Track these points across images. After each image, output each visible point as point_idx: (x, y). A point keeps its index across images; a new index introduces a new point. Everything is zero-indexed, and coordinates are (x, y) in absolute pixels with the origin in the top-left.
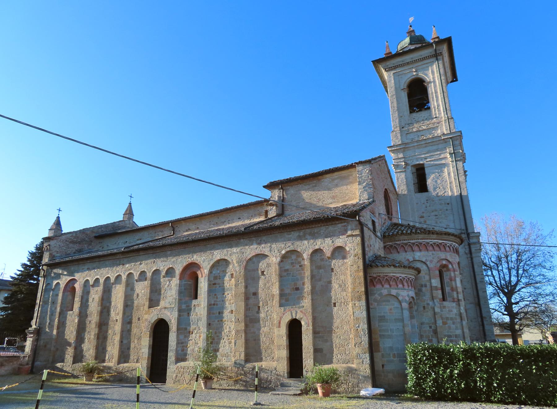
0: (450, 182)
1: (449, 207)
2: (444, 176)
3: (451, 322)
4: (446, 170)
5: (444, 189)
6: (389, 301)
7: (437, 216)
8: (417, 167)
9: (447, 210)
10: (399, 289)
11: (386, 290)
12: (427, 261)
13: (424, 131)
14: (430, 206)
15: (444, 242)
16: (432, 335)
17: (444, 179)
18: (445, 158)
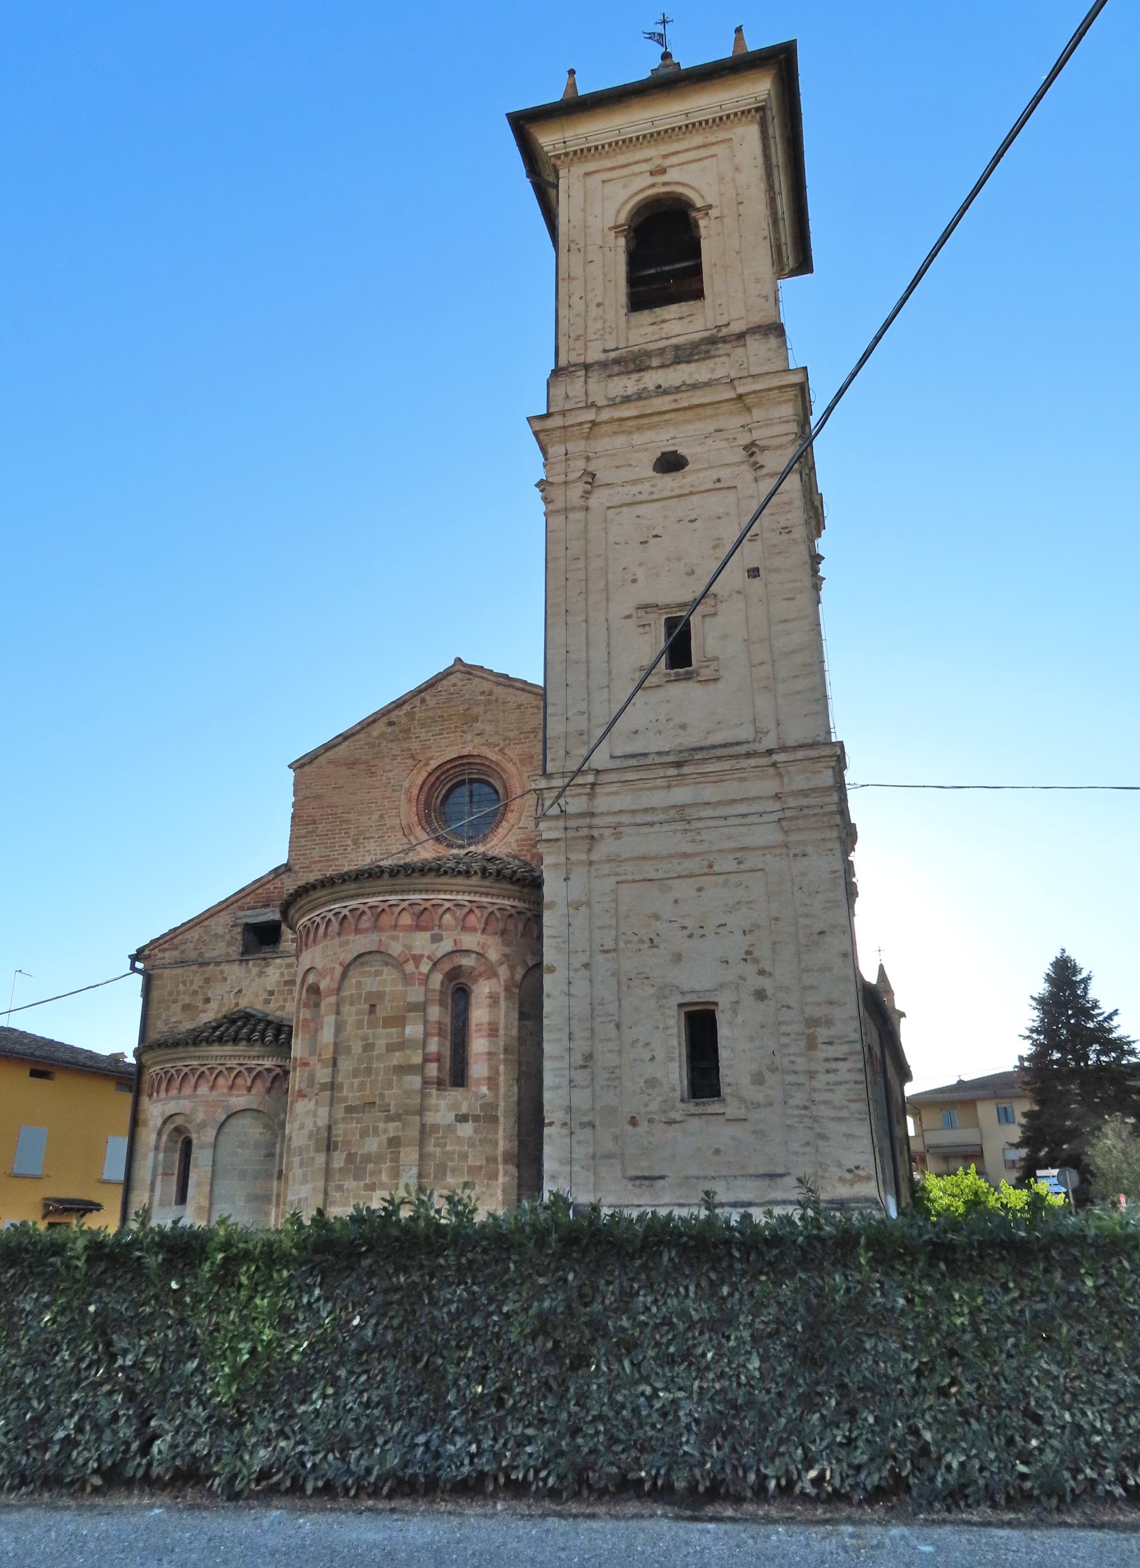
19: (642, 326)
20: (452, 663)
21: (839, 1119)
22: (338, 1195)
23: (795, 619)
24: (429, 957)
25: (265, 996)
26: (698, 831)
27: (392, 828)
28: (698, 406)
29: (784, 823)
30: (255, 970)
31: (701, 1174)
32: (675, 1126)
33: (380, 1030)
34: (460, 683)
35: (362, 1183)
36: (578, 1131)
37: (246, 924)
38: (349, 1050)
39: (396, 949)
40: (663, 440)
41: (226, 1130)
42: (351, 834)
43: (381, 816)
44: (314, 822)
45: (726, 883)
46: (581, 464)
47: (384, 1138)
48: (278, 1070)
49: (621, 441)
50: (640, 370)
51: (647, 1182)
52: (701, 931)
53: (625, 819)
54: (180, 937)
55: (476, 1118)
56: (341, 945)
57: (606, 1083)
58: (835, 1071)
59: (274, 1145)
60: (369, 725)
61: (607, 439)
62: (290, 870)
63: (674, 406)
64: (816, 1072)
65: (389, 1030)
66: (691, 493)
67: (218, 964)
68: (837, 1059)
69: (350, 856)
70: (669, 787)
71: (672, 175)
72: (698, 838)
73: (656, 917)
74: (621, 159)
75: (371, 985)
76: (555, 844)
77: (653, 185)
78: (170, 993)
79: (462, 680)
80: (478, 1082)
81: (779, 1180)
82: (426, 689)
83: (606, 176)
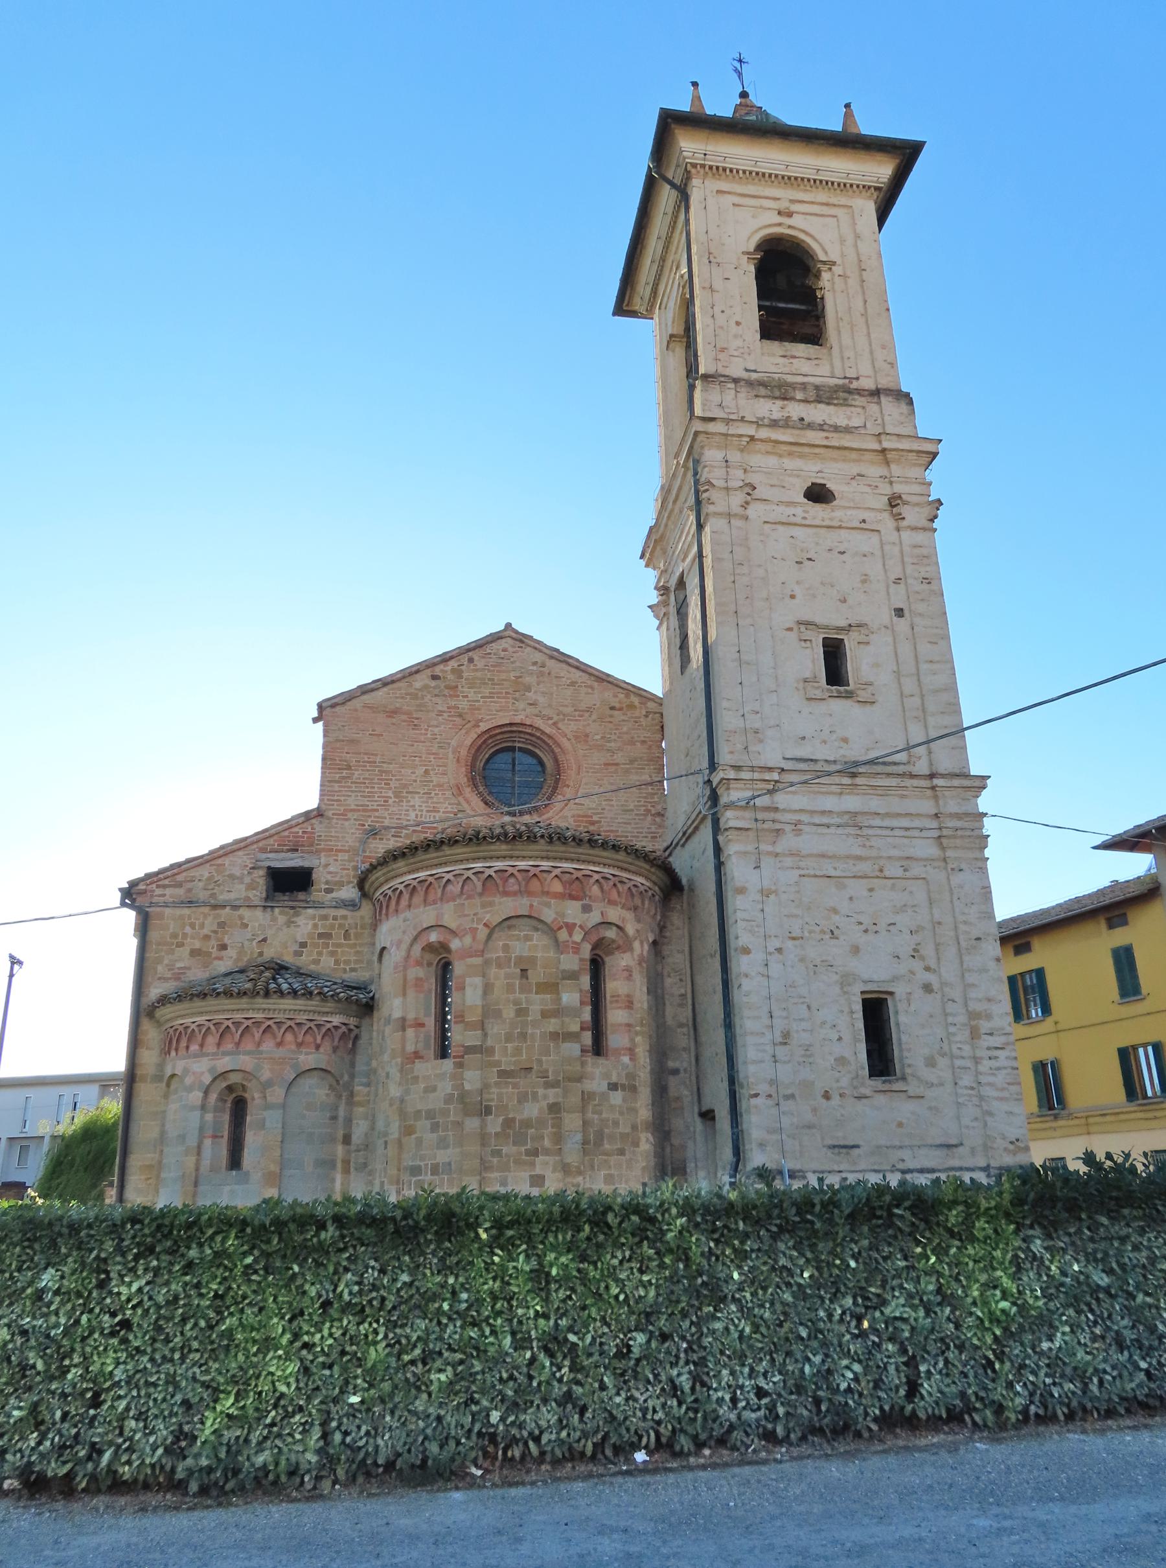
15: (434, 872)
19: (774, 355)
20: (502, 628)
21: (1001, 1099)
22: (495, 1160)
23: (938, 662)
24: (581, 927)
25: (296, 947)
26: (868, 837)
27: (440, 785)
28: (846, 448)
29: (944, 841)
30: (282, 919)
31: (888, 1144)
32: (864, 1101)
33: (533, 996)
34: (511, 649)
35: (523, 1149)
36: (782, 1102)
37: (269, 868)
38: (498, 1014)
39: (548, 915)
40: (814, 471)
41: (293, 1090)
42: (392, 785)
43: (426, 772)
44: (349, 767)
45: (893, 887)
46: (740, 473)
47: (544, 1104)
48: (344, 1028)
49: (772, 461)
50: (785, 399)
51: (844, 1151)
52: (875, 928)
53: (805, 818)
54: (184, 874)
55: (623, 1087)
56: (483, 906)
57: (802, 1059)
58: (996, 1058)
59: (337, 1108)
60: (411, 674)
61: (759, 456)
62: (322, 815)
63: (825, 443)
64: (981, 1058)
65: (542, 996)
66: (840, 527)
67: (235, 908)
68: (996, 1048)
69: (391, 809)
70: (841, 793)
71: (796, 221)
72: (868, 844)
73: (835, 911)
74: (751, 189)
75: (519, 949)
76: (744, 833)
77: (780, 225)
78: (174, 936)
79: (513, 647)
80: (618, 1052)
81: (955, 1150)
82: (474, 649)
83: (737, 200)
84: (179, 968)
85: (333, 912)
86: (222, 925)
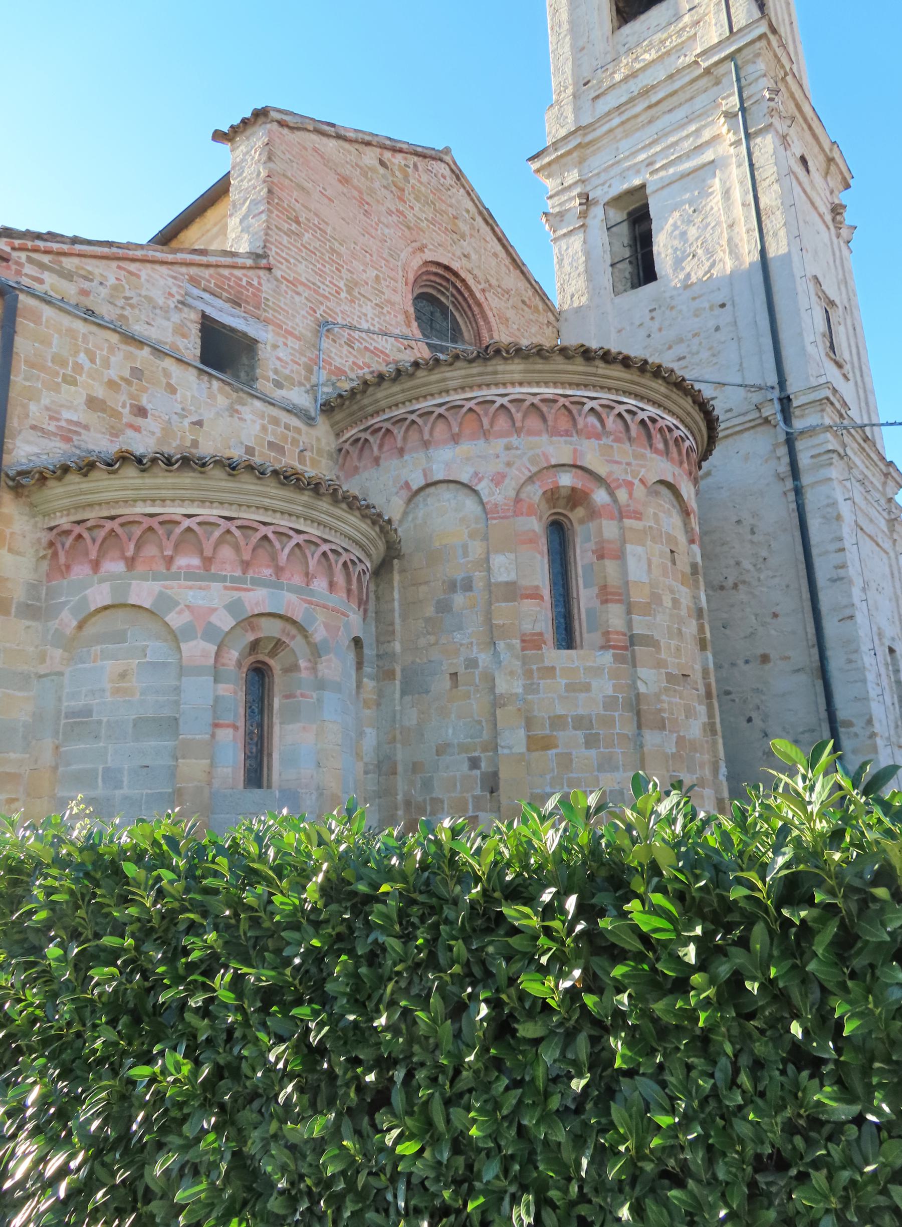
0: (730, 222)
1: (725, 316)
2: (712, 208)
3: (580, 735)
4: (716, 184)
5: (710, 253)
6: (120, 637)
7: (684, 358)
8: (631, 208)
9: (717, 329)
10: (175, 576)
11: (106, 587)
12: (480, 480)
13: (649, 72)
14: (660, 330)
16: (476, 798)
17: (709, 220)
18: (716, 138)
54: (76, 261)
84: (69, 421)
85: (285, 418)
86: (137, 373)
